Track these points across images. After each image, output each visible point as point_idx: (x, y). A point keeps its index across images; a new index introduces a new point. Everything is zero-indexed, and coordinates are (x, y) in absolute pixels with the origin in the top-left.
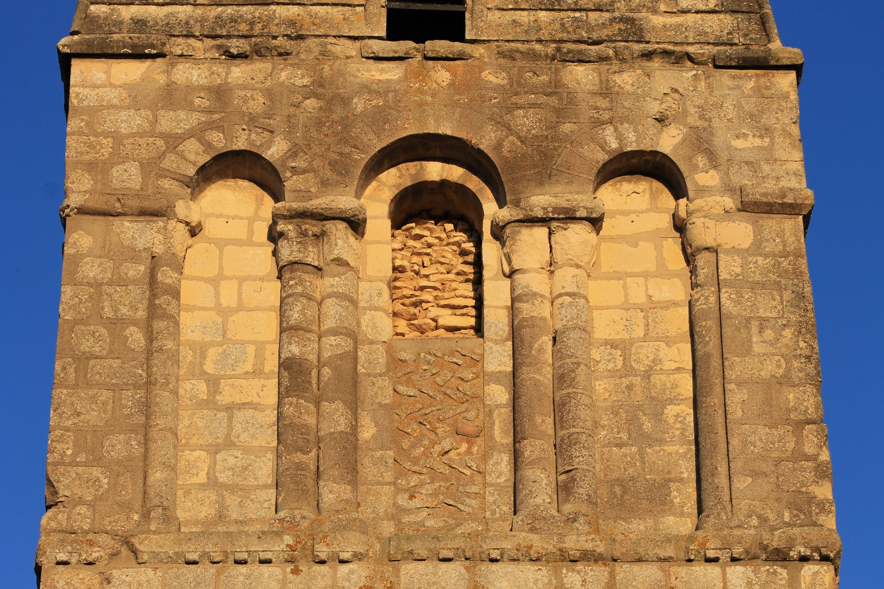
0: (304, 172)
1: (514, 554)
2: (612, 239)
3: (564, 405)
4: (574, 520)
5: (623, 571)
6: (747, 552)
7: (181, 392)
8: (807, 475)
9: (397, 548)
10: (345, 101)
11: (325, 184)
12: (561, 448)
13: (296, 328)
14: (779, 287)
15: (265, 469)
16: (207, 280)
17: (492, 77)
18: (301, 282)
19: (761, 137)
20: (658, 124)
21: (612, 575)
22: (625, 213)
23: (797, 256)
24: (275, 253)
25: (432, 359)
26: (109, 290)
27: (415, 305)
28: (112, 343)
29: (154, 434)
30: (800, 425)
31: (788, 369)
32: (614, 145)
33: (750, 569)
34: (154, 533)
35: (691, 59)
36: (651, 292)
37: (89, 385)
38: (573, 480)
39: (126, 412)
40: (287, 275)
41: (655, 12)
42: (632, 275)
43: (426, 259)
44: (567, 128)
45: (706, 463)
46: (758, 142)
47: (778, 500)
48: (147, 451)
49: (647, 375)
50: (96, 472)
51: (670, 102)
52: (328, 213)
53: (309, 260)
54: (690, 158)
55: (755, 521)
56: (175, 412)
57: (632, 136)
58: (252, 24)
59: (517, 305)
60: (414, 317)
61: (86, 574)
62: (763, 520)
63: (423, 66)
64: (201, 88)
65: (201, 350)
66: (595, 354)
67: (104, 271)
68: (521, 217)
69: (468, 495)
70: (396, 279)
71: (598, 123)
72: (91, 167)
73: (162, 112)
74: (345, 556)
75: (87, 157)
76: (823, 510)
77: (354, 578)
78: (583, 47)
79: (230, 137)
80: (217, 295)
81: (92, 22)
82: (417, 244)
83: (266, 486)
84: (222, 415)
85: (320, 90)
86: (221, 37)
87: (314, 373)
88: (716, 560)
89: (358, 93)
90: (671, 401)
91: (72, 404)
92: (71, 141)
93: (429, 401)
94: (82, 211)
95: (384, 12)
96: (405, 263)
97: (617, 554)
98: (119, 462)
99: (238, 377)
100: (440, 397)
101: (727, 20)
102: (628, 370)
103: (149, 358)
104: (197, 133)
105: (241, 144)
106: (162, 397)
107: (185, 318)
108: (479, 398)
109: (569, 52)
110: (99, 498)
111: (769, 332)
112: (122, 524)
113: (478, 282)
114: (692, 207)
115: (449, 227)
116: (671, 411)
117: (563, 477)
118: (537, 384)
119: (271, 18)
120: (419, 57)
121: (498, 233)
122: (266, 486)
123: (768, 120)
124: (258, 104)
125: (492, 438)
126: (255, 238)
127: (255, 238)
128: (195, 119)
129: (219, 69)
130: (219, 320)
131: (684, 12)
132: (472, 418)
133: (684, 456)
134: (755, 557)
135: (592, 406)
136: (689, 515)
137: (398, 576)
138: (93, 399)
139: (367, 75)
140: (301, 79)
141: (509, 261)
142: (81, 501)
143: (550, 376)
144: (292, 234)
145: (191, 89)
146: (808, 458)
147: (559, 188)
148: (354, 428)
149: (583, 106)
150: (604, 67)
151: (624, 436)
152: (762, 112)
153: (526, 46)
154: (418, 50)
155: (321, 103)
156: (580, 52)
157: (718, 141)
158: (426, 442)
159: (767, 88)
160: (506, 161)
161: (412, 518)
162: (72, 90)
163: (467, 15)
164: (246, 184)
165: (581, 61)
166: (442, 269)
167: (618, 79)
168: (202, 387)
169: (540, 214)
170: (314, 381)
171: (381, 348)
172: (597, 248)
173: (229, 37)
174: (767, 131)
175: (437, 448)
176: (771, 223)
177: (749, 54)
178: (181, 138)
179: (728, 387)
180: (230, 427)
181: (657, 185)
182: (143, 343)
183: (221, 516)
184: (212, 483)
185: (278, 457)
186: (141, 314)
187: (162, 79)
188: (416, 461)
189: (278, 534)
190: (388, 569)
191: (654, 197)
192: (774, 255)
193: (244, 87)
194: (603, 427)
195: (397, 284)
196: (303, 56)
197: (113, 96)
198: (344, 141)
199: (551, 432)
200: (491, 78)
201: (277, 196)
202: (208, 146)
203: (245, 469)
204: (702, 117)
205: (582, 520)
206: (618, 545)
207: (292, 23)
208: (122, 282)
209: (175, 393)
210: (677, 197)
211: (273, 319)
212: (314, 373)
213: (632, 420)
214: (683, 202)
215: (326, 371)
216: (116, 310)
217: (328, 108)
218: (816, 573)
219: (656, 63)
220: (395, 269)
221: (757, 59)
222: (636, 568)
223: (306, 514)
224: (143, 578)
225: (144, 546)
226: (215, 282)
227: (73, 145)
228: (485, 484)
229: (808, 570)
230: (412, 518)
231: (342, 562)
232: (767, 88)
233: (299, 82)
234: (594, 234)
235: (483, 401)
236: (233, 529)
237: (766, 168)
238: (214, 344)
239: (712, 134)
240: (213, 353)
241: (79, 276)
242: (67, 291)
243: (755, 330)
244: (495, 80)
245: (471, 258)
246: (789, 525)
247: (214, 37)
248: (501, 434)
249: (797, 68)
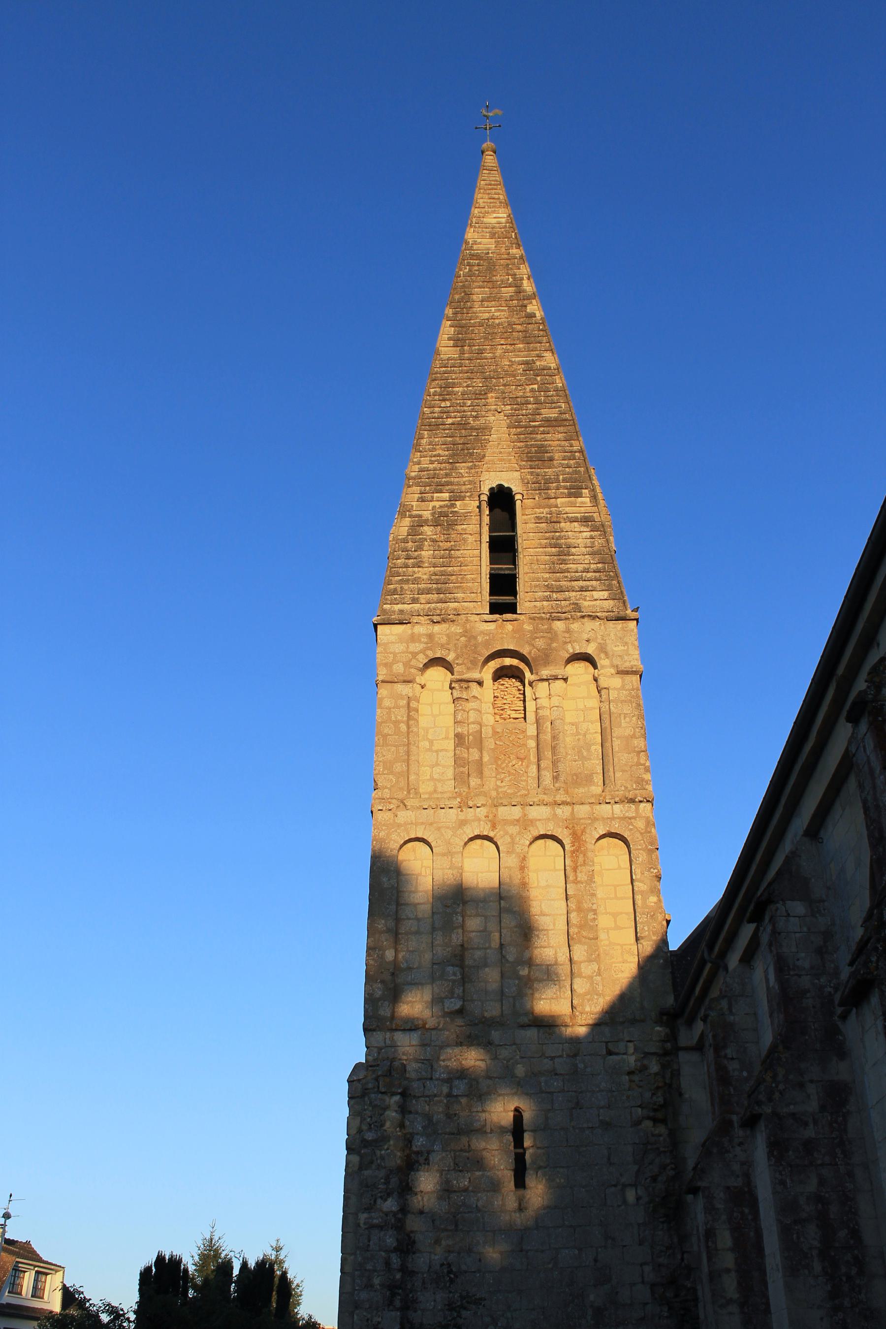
0: (461, 664)
1: (538, 803)
2: (572, 685)
3: (555, 747)
4: (559, 790)
5: (576, 807)
6: (620, 800)
7: (420, 746)
8: (642, 771)
9: (497, 802)
10: (475, 638)
11: (468, 669)
12: (555, 763)
13: (460, 722)
14: (631, 702)
15: (450, 773)
16: (428, 704)
17: (528, 627)
18: (461, 705)
19: (624, 646)
20: (587, 643)
21: (573, 809)
22: (576, 675)
23: (638, 690)
24: (452, 694)
25: (508, 731)
26: (394, 710)
27: (502, 710)
28: (395, 730)
29: (410, 762)
30: (639, 752)
31: (634, 732)
32: (571, 651)
33: (622, 805)
34: (412, 798)
35: (598, 618)
36: (585, 704)
37: (387, 745)
38: (559, 775)
39: (401, 754)
40: (456, 703)
41: (585, 600)
42: (579, 698)
43: (506, 693)
44: (554, 645)
45: (606, 767)
46: (623, 648)
47: (631, 780)
48: (408, 769)
49: (585, 735)
50: (391, 777)
51: (592, 634)
52: (470, 680)
53: (464, 697)
54: (599, 655)
55: (623, 788)
56: (418, 754)
57: (577, 647)
58: (441, 610)
59: (538, 711)
60: (502, 714)
61: (389, 813)
62: (626, 788)
63: (502, 624)
64: (424, 635)
65: (427, 730)
66: (566, 728)
67: (391, 703)
68: (538, 679)
69: (522, 781)
70: (495, 701)
71: (566, 643)
72: (386, 665)
73: (410, 644)
74: (478, 805)
75: (384, 661)
76: (647, 783)
77: (482, 813)
78: (559, 614)
79: (434, 653)
80: (432, 710)
81: (384, 612)
82: (502, 687)
83: (451, 779)
84: (434, 754)
85: (466, 634)
86: (430, 615)
87: (466, 738)
88: (610, 803)
89: (480, 635)
90: (593, 744)
91: (382, 752)
92: (378, 656)
93: (507, 746)
94: (383, 682)
95: (488, 603)
96: (498, 695)
97: (574, 802)
98: (399, 773)
99: (439, 740)
100: (511, 745)
101: (611, 602)
102: (578, 733)
103: (408, 735)
104: (423, 651)
105: (438, 655)
106: (413, 748)
107: (421, 719)
108: (525, 745)
109: (555, 617)
110: (392, 786)
111: (627, 718)
112: (400, 796)
113: (524, 701)
114: (599, 673)
115: (514, 680)
116: (593, 748)
117: (555, 774)
118: (545, 740)
119: (448, 608)
120: (501, 621)
121: (531, 684)
122: (451, 779)
123: (626, 639)
124: (444, 640)
125: (530, 759)
126: (444, 689)
127: (444, 689)
128: (422, 646)
129: (430, 627)
130: (433, 719)
131: (595, 600)
132: (522, 752)
133: (598, 764)
134: (624, 801)
135: (565, 747)
136: (600, 786)
137: (497, 812)
138: (389, 750)
139: (482, 628)
140: (459, 630)
141: (535, 695)
142: (386, 788)
143: (550, 737)
144: (457, 688)
145: (420, 635)
146: (642, 765)
147: (551, 668)
148: (481, 758)
149: (560, 637)
150: (567, 622)
151: (577, 757)
152: (624, 636)
153: (539, 615)
154: (500, 618)
155: (466, 639)
156: (558, 616)
157: (609, 648)
158: (507, 762)
159: (626, 628)
160: (533, 658)
161: (502, 789)
162: (378, 637)
163: (518, 604)
164: (441, 668)
165: (559, 620)
166: (512, 696)
167: (572, 626)
168: (427, 743)
169: (545, 678)
170: (467, 741)
171: (490, 728)
172: (566, 689)
173: (433, 615)
174: (626, 644)
175: (511, 764)
176: (628, 678)
177: (619, 615)
178: (417, 654)
179: (613, 739)
180: (438, 758)
181: (588, 664)
182: (406, 729)
183: (435, 791)
184: (432, 779)
185: (455, 769)
186: (405, 719)
187: (410, 632)
188: (503, 769)
189: (455, 798)
190: (494, 810)
191: (586, 668)
192: (629, 690)
193: (439, 634)
194: (569, 754)
195: (496, 702)
196: (459, 621)
197: (393, 638)
198: (475, 653)
199: (551, 757)
200: (527, 627)
201: (453, 674)
202: (427, 656)
203: (443, 773)
204: (602, 639)
205: (562, 789)
206: (574, 799)
207: (455, 609)
208: (398, 707)
209: (418, 747)
210: (595, 669)
211: (452, 718)
212: (466, 738)
213: (580, 752)
214: (596, 670)
215: (471, 737)
216: (396, 718)
217: (469, 640)
218: (645, 807)
219: (586, 619)
220: (494, 697)
221: (622, 617)
222: (581, 806)
223: (465, 790)
224: (409, 815)
225: (409, 803)
226: (431, 705)
227: (379, 658)
228: (528, 777)
229: (642, 805)
230: (502, 789)
231: (478, 807)
232: (626, 628)
233: (458, 631)
234: (565, 684)
235: (526, 746)
236: (439, 796)
237: (626, 658)
238: (431, 728)
239: (606, 646)
240: (431, 731)
241: (383, 705)
242: (379, 711)
243: (622, 718)
244: (528, 628)
245: (522, 692)
246: (635, 789)
247: (428, 616)
248: (533, 758)
249: (637, 620)
